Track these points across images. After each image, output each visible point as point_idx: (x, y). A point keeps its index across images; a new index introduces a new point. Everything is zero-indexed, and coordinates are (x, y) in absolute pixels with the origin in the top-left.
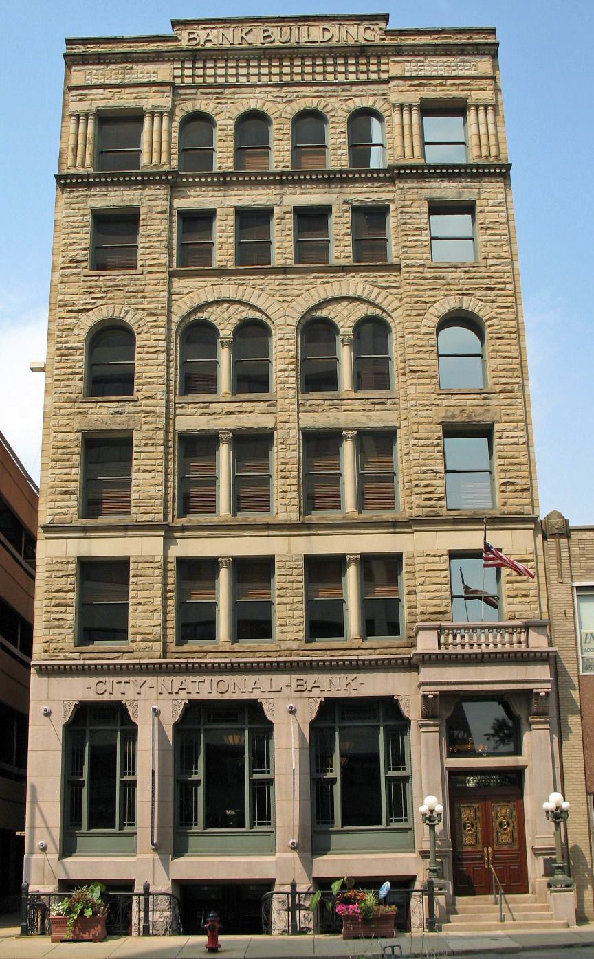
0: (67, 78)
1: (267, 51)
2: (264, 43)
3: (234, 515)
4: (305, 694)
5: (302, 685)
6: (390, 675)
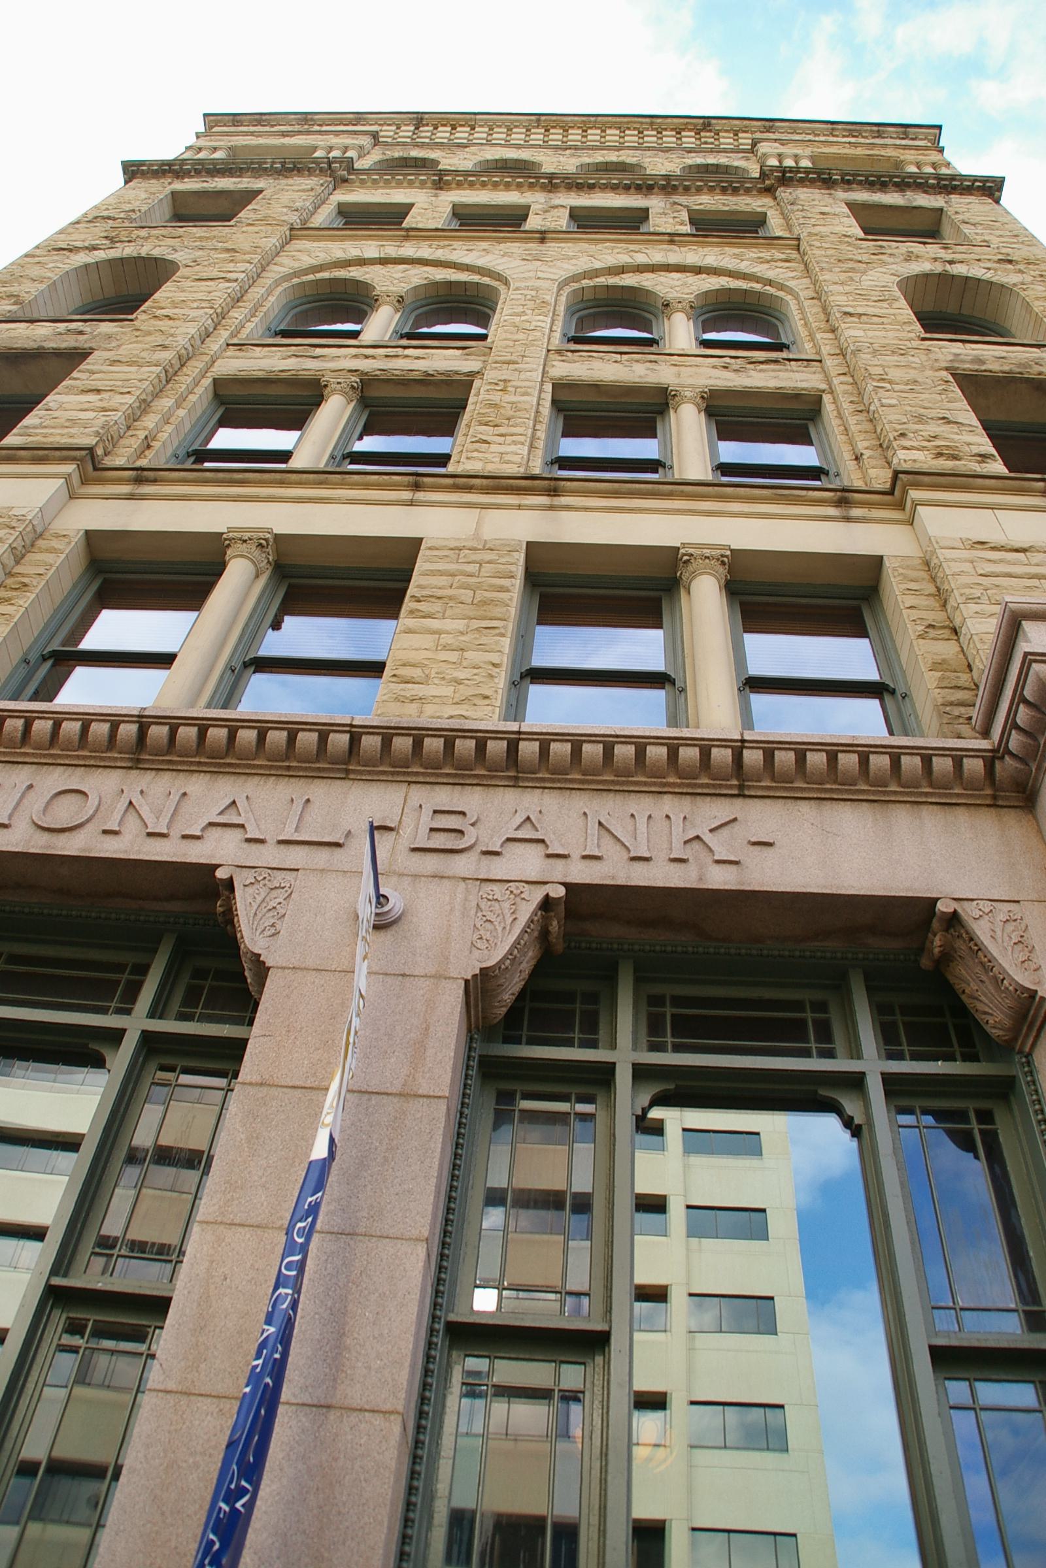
0: (523, 643)
1: (543, 118)
2: (200, 149)
3: (520, 1110)
4: (463, 865)
5: (461, 832)
6: (902, 819)
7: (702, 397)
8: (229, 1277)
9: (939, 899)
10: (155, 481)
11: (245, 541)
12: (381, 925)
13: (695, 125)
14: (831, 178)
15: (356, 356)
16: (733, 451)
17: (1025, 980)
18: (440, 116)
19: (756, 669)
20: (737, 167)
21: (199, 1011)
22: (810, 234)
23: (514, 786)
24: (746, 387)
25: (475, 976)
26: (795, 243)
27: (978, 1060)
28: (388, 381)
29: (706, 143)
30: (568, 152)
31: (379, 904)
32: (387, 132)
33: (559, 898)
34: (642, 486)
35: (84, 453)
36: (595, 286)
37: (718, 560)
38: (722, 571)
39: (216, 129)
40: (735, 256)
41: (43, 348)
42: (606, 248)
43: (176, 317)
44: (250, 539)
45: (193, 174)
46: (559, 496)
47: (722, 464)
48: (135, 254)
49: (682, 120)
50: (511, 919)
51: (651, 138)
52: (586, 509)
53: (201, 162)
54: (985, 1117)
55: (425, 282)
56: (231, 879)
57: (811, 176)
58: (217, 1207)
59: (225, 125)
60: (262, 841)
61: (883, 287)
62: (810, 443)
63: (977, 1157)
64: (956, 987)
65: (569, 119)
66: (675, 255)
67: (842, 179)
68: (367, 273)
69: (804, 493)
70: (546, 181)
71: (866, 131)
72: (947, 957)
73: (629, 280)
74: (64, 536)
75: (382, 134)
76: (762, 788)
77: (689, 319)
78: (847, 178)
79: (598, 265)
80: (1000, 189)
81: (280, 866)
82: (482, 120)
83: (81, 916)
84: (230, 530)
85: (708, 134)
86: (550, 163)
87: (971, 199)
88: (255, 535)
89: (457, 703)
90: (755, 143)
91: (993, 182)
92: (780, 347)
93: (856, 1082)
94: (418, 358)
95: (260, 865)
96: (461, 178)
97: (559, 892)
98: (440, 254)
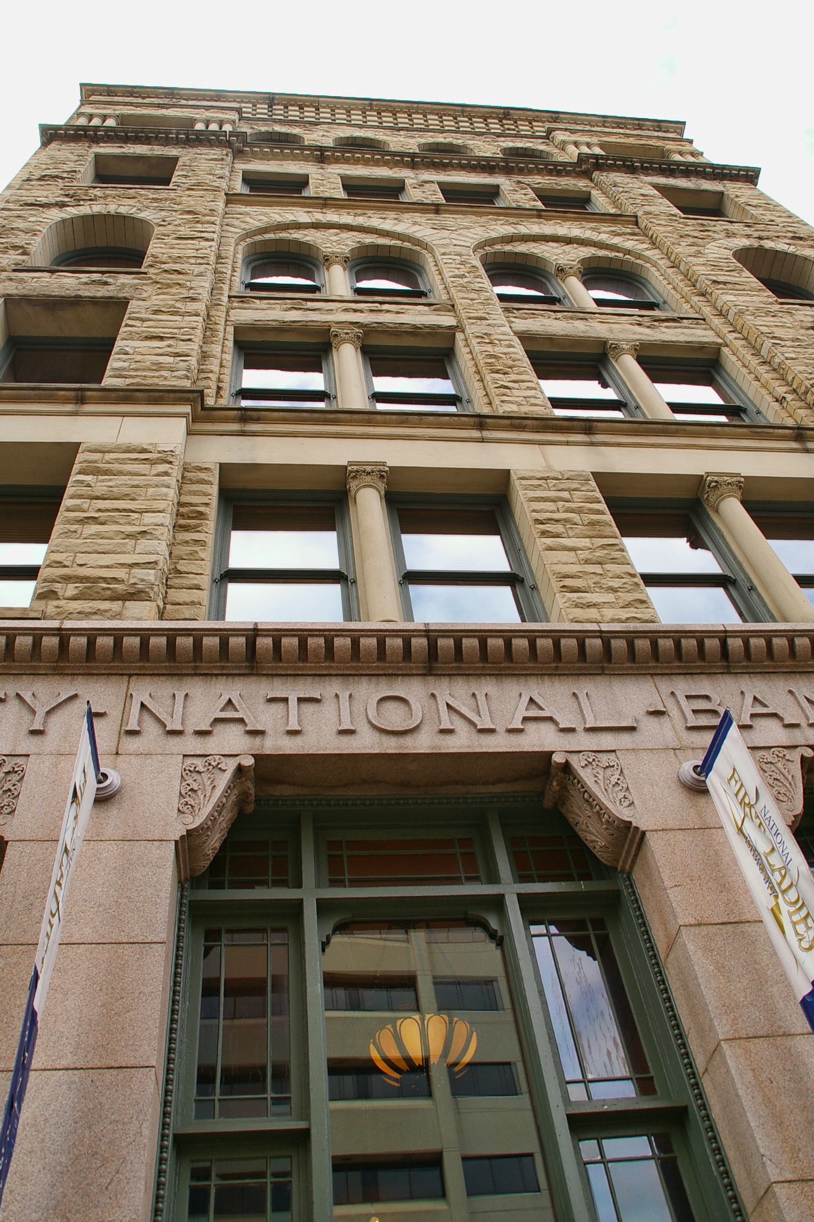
1: (375, 103)
7: (636, 350)
8: (772, 1079)
9: (553, 752)
10: (258, 420)
11: (368, 473)
12: (103, 799)
13: (497, 114)
14: (633, 165)
15: (346, 310)
16: (385, 384)
17: (625, 814)
18: (289, 97)
19: (414, 564)
20: (541, 151)
21: (534, 872)
22: (647, 213)
23: (728, 673)
24: (664, 341)
25: (182, 837)
26: (634, 219)
27: (591, 879)
28: (384, 332)
29: (509, 129)
30: (402, 133)
31: (99, 782)
32: (247, 108)
33: (249, 766)
34: (655, 426)
35: (195, 395)
36: (495, 252)
37: (737, 485)
38: (382, 486)
39: (92, 98)
40: (593, 229)
41: (80, 296)
42: (490, 219)
43: (184, 271)
44: (373, 472)
45: (106, 139)
46: (593, 434)
47: (243, 389)
48: (104, 212)
49: (486, 110)
50: (211, 787)
51: (388, 119)
52: (619, 445)
53: (84, 128)
54: (599, 924)
55: (358, 245)
56: (567, 761)
57: (618, 163)
58: (728, 1026)
59: (101, 95)
60: (491, 731)
61: (725, 259)
62: (321, 372)
63: (595, 959)
64: (571, 820)
65: (396, 104)
66: (332, 216)
67: (642, 166)
68: (306, 235)
69: (771, 430)
70: (409, 159)
71: (629, 124)
72: (563, 797)
73: (522, 248)
74: (206, 469)
75: (244, 110)
76: (787, 667)
77: (345, 269)
78: (645, 165)
79: (494, 235)
80: (757, 177)
81: (599, 749)
82: (324, 102)
83: (408, 803)
84: (351, 463)
85: (509, 122)
86: (397, 142)
87: (739, 185)
88: (376, 468)
89: (623, 607)
90: (550, 131)
91: (753, 171)
92: (552, 301)
93: (497, 903)
94: (398, 313)
95: (584, 749)
96: (339, 154)
97: (249, 762)
98: (360, 221)
